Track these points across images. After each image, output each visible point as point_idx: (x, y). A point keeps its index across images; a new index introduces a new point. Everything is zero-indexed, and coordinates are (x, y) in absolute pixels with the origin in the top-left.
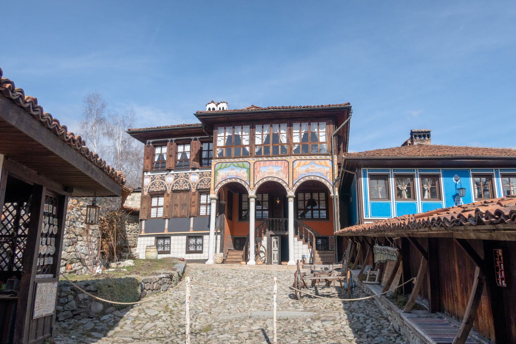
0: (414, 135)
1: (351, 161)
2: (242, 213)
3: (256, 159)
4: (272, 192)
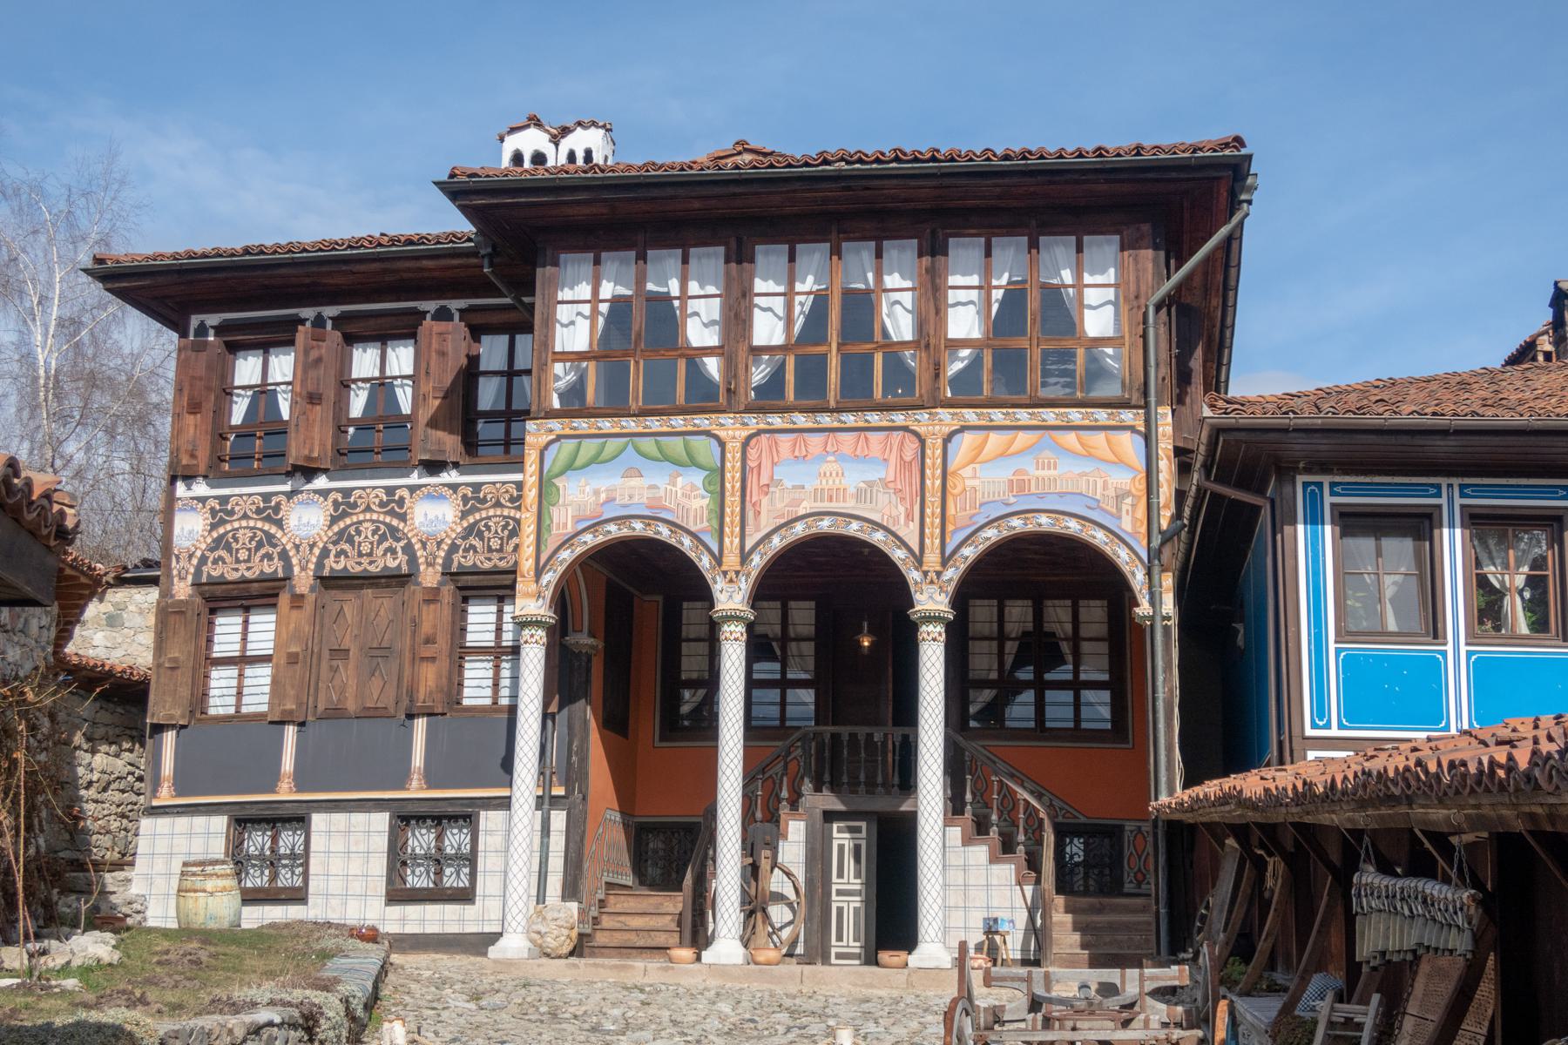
1: (1242, 436)
3: (754, 422)
4: (836, 593)
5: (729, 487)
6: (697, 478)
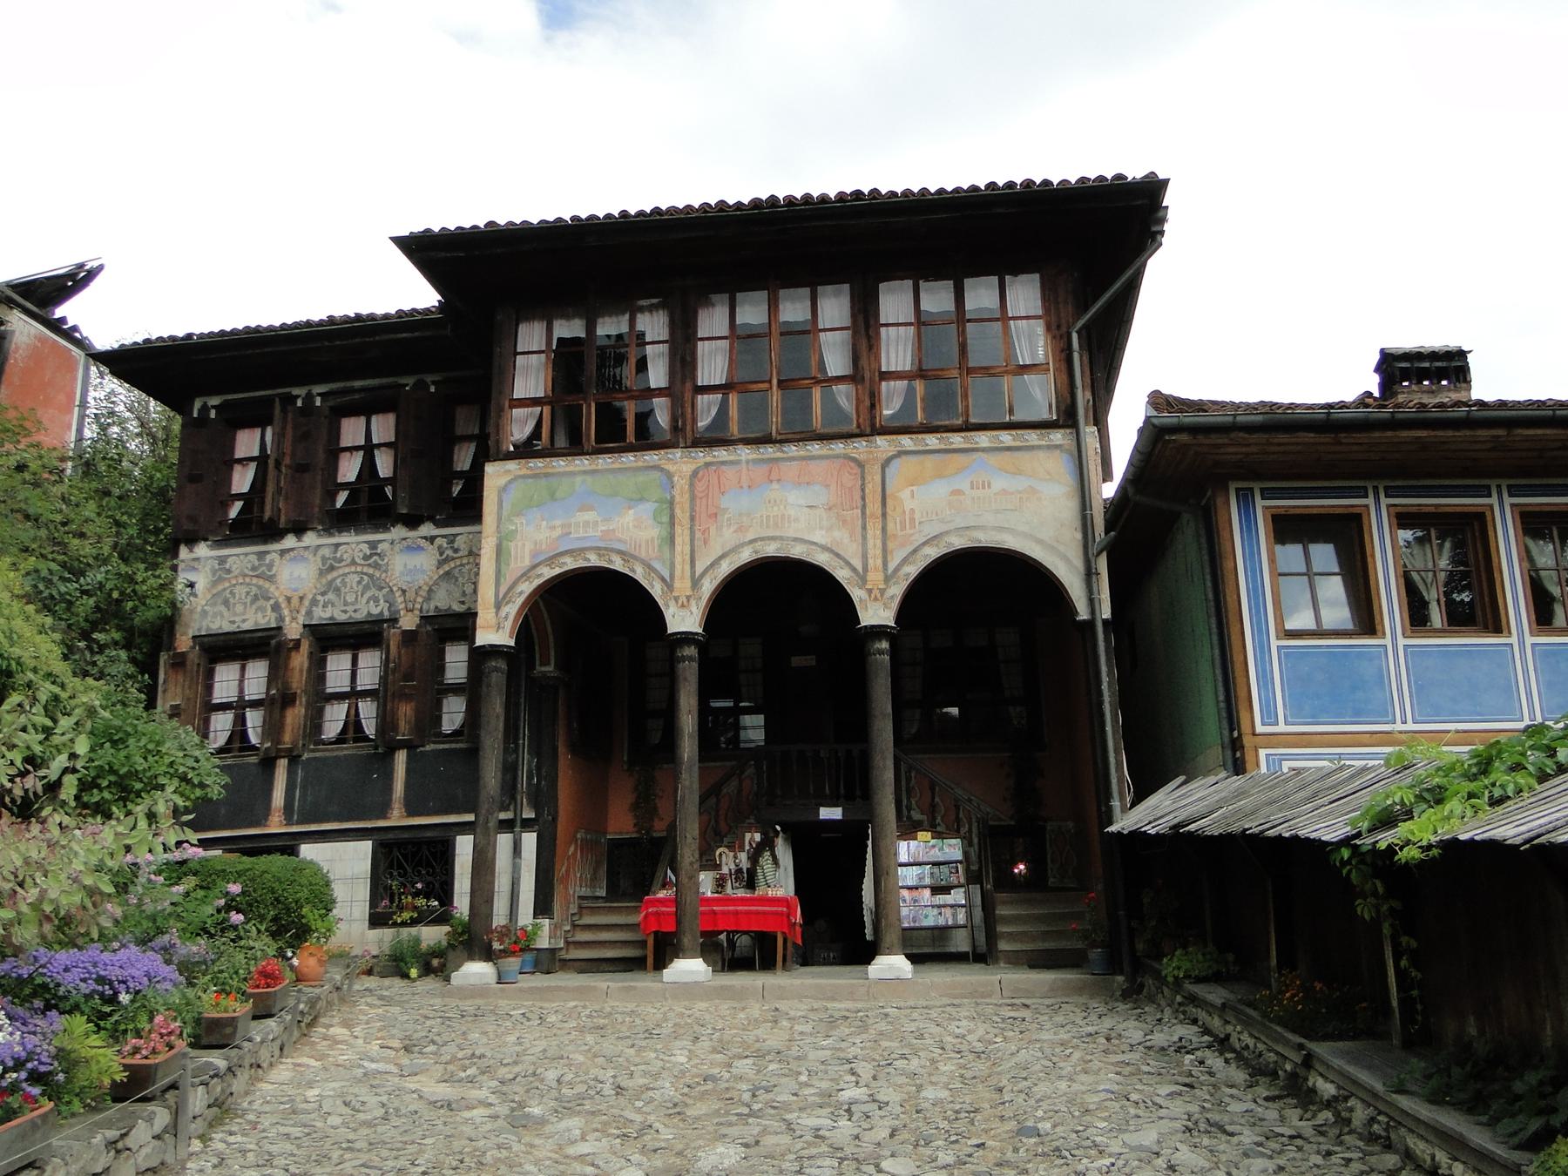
0: (1394, 367)
1: (1184, 438)
5: (874, 506)
6: (648, 508)
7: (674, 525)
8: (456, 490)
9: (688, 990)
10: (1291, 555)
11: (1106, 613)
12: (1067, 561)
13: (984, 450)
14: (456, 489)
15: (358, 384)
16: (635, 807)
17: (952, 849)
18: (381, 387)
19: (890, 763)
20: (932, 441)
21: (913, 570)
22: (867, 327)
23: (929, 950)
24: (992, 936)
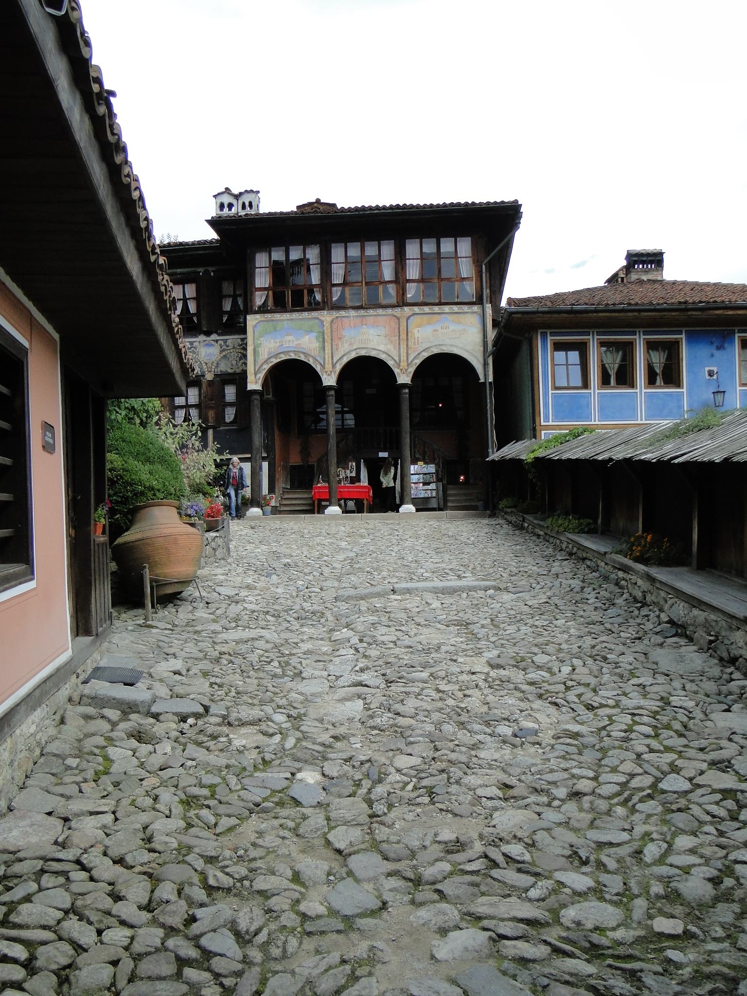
1: (519, 316)
2: (305, 242)
5: (403, 335)
7: (326, 341)
8: (225, 319)
9: (333, 517)
10: (560, 356)
11: (491, 379)
12: (476, 357)
13: (447, 313)
14: (225, 319)
15: (179, 271)
16: (301, 452)
17: (432, 468)
18: (188, 273)
19: (408, 435)
20: (426, 309)
21: (418, 362)
22: (401, 260)
23: (422, 505)
24: (445, 501)
